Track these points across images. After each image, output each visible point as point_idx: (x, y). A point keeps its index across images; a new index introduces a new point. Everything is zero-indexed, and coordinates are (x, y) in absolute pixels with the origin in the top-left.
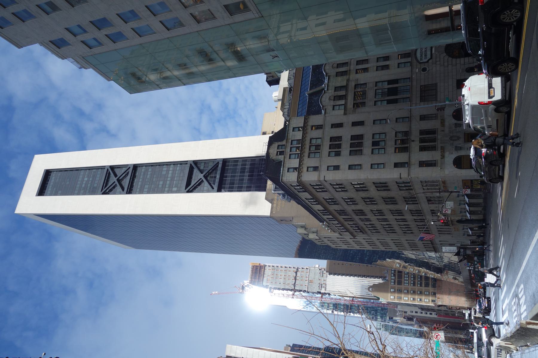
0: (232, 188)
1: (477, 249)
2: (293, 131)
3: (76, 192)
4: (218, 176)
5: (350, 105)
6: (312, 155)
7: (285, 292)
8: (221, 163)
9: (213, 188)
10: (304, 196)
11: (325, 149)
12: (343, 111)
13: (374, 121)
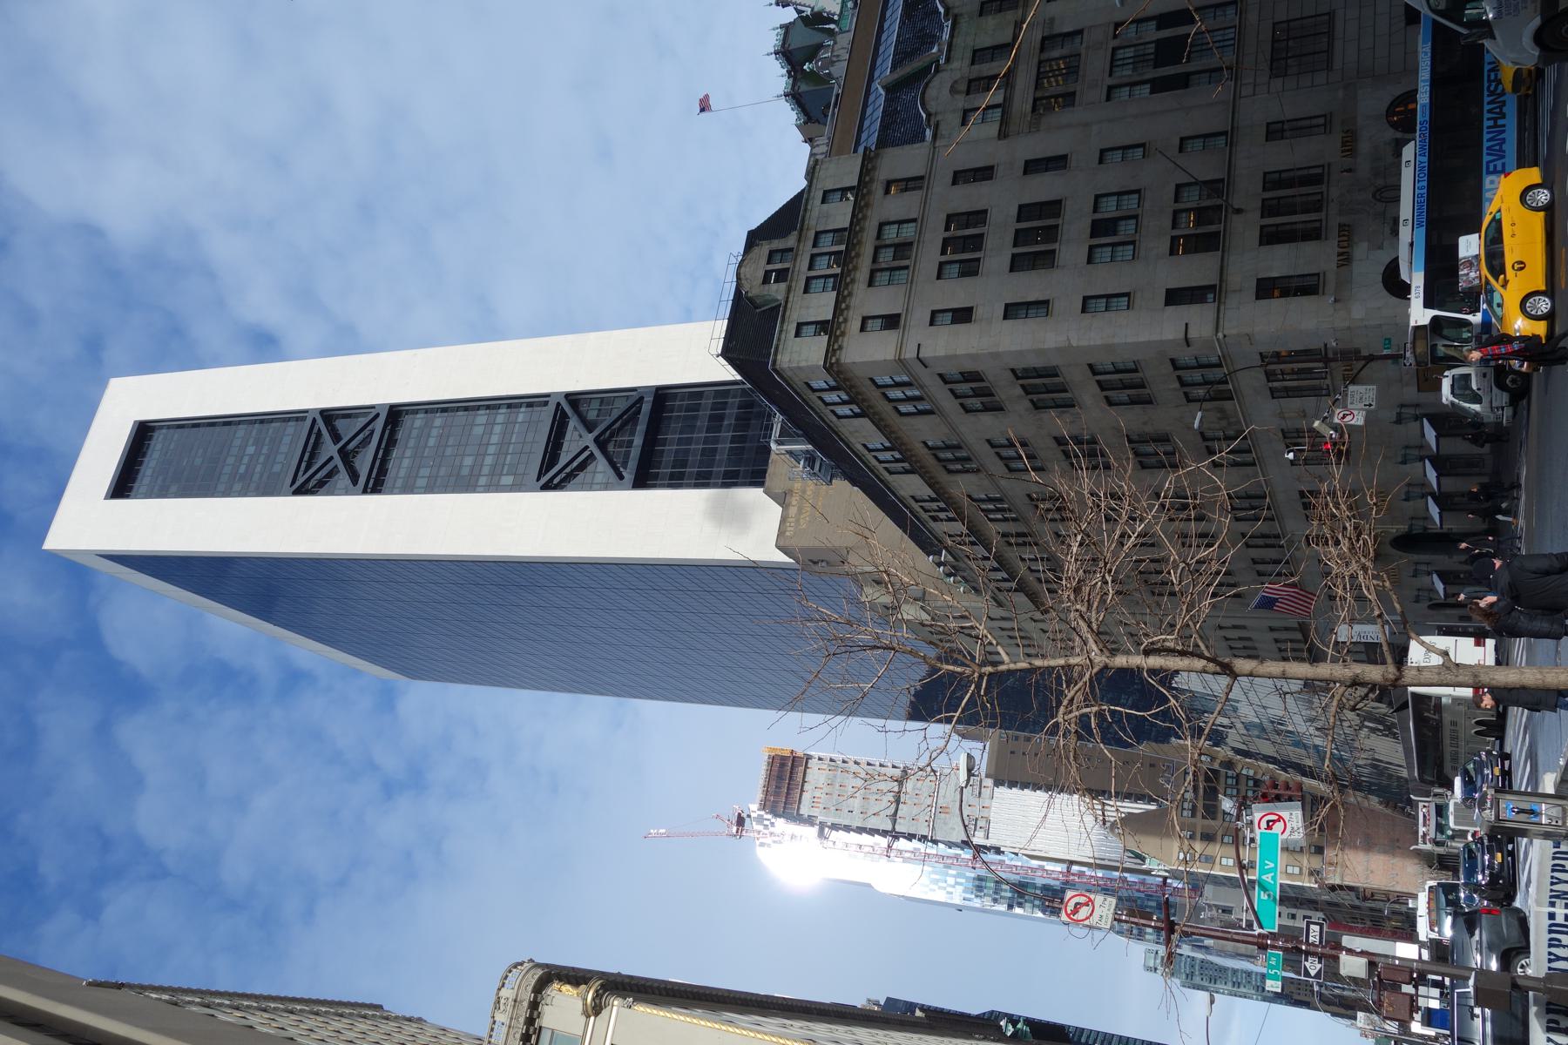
1: (1462, 596)
2: (824, 201)
3: (221, 487)
4: (638, 441)
5: (1023, 100)
6: (883, 277)
7: (865, 839)
8: (649, 399)
9: (621, 477)
10: (862, 434)
11: (929, 255)
12: (996, 126)
13: (1103, 152)
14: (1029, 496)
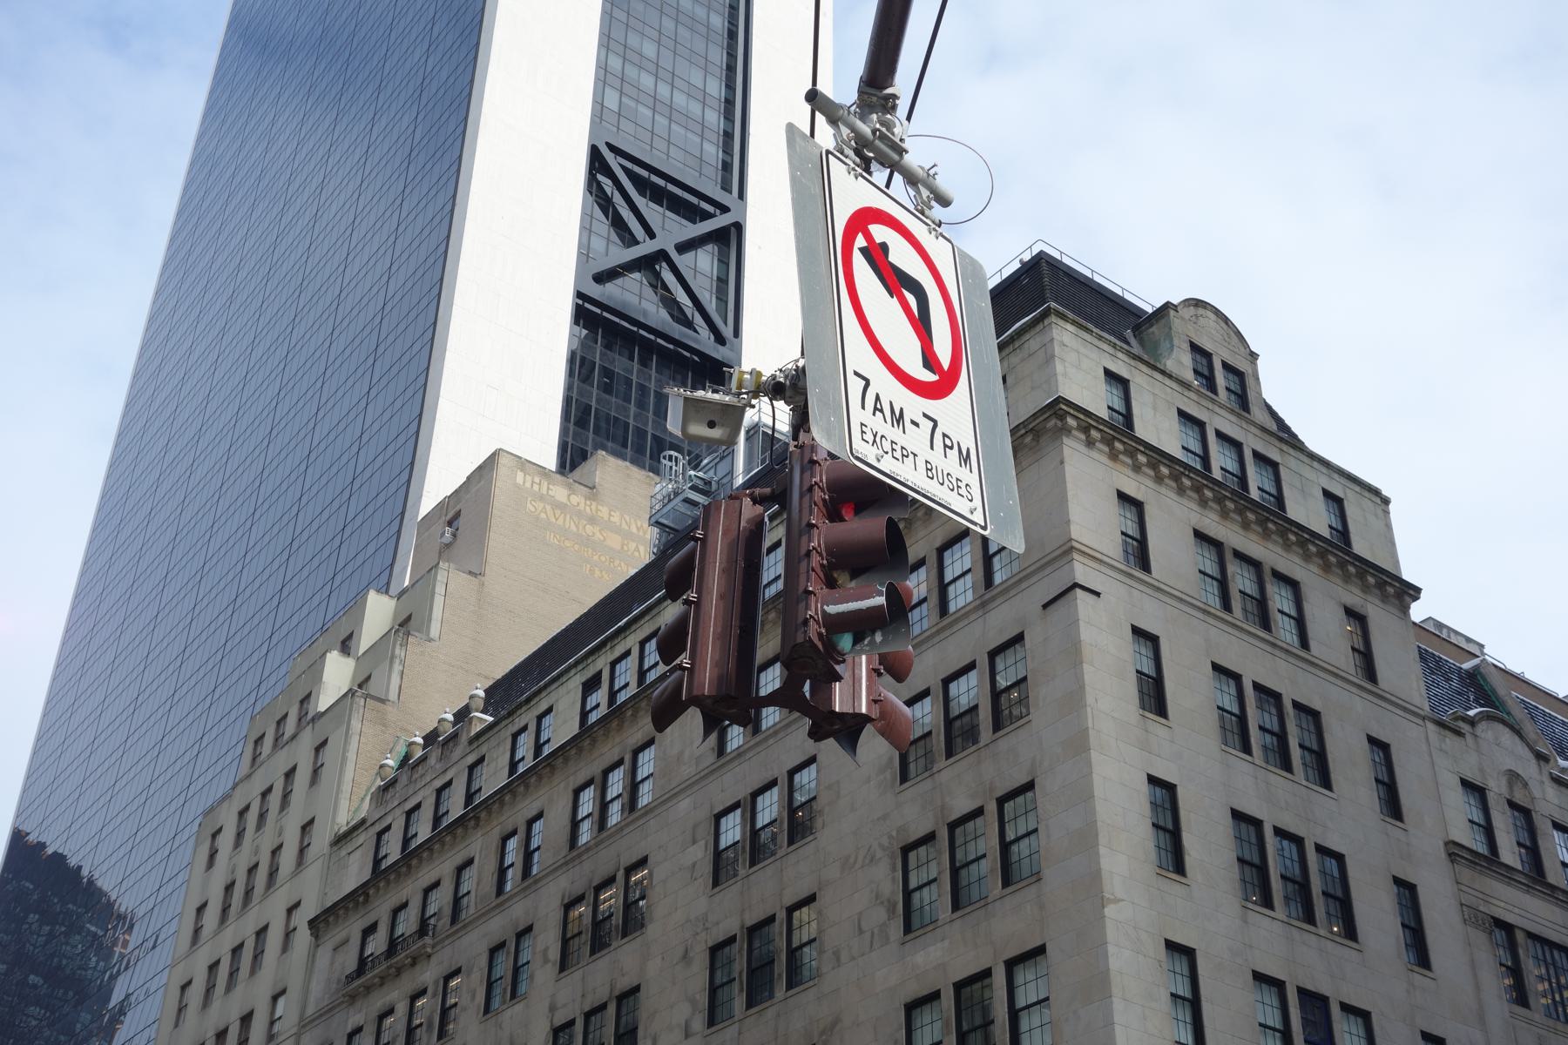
0: (586, 378)
14: (642, 862)
